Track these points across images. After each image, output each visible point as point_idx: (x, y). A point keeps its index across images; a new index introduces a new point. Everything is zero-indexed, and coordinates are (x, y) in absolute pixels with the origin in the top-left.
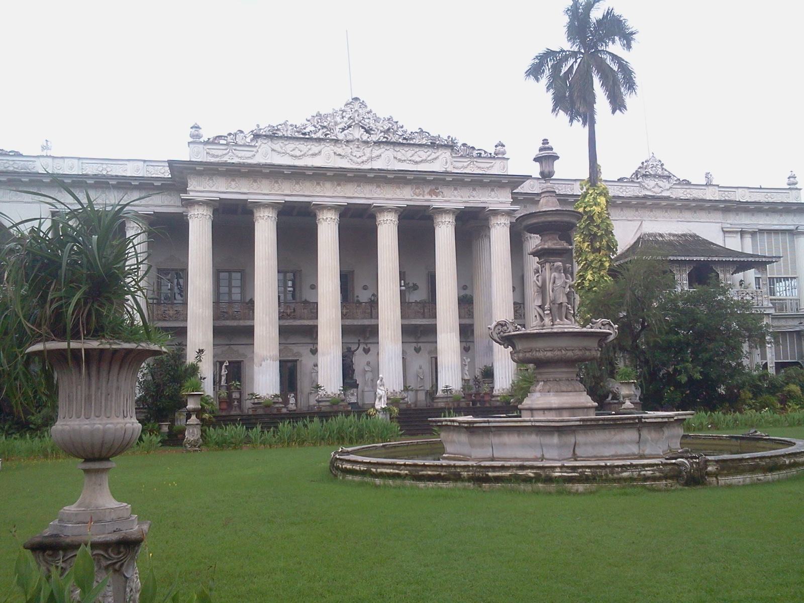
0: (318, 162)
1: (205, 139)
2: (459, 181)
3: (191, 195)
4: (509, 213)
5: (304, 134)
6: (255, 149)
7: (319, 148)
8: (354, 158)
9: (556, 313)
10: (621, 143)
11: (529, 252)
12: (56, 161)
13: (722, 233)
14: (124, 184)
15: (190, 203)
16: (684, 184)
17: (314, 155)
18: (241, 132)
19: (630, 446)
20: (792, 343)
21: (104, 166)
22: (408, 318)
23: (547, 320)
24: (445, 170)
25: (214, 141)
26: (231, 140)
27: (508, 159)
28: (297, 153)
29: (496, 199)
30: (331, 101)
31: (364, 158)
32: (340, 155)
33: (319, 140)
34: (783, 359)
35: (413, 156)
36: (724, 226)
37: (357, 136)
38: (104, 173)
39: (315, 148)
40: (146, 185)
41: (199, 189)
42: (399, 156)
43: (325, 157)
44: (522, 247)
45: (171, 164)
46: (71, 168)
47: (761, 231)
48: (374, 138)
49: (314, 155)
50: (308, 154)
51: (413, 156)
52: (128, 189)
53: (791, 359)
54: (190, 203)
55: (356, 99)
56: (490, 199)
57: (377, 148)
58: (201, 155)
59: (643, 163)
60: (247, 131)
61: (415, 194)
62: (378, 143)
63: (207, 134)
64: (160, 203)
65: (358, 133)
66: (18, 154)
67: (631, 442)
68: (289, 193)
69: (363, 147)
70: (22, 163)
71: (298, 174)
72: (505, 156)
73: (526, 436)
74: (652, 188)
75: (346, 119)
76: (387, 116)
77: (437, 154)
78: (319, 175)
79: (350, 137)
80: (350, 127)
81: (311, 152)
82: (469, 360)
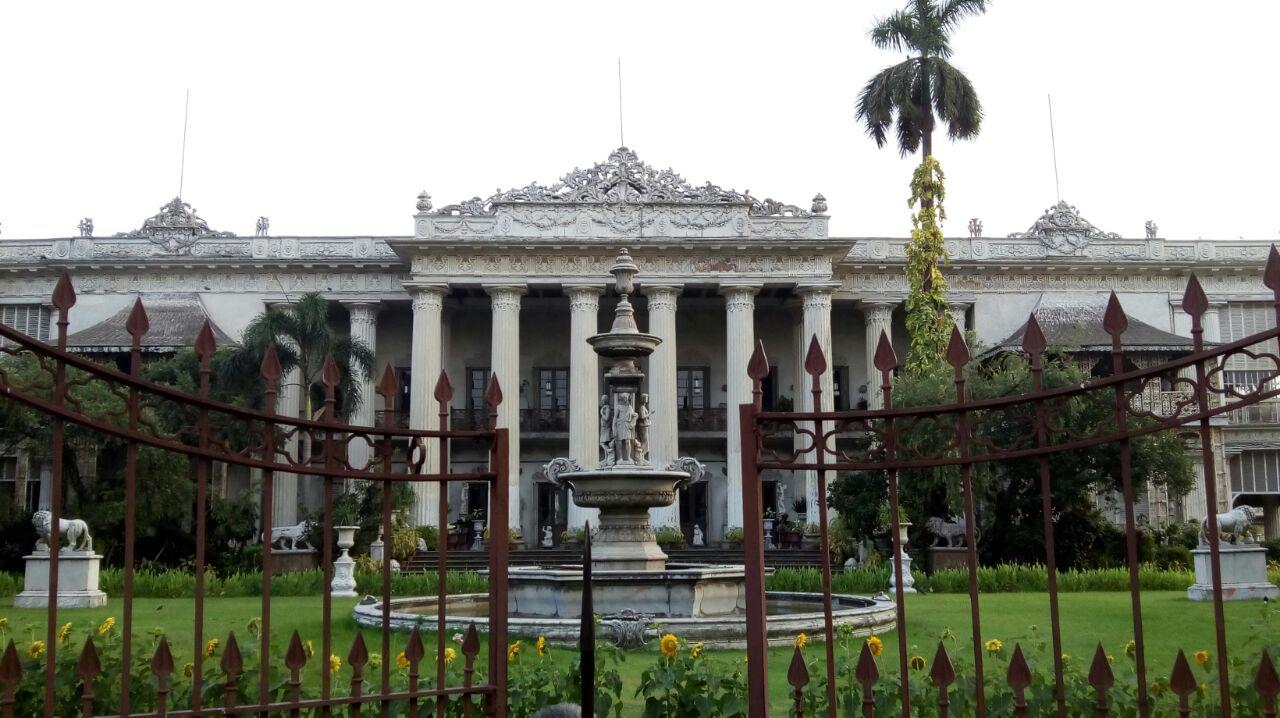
0: (570, 233)
1: (434, 209)
2: (758, 251)
3: (417, 281)
4: (827, 291)
5: (556, 198)
6: (493, 220)
7: (574, 214)
8: (618, 226)
9: (620, 451)
10: (992, 189)
11: (1121, 298)
12: (273, 242)
13: (1167, 309)
14: (346, 268)
15: (415, 291)
16: (1111, 240)
17: (565, 224)
18: (478, 199)
19: (657, 605)
20: (1260, 468)
21: (327, 246)
22: (695, 427)
23: (610, 459)
24: (738, 235)
25: (445, 213)
26: (470, 209)
27: (828, 218)
28: (546, 222)
29: (809, 272)
30: (594, 153)
31: (631, 225)
32: (600, 222)
33: (573, 205)
34: (1270, 490)
35: (696, 219)
36: (1172, 297)
37: (623, 197)
38: (326, 253)
39: (566, 215)
40: (370, 268)
41: (427, 273)
42: (678, 218)
43: (584, 227)
44: (865, 333)
45: (392, 242)
46: (288, 249)
47: (1235, 304)
48: (645, 199)
49: (565, 224)
50: (559, 222)
51: (696, 219)
52: (353, 272)
53: (1257, 490)
54: (415, 291)
55: (623, 149)
56: (802, 272)
57: (649, 210)
58: (430, 234)
59: (1047, 211)
60: (484, 198)
61: (698, 269)
62: (650, 205)
63: (437, 204)
64: (388, 289)
65: (622, 193)
66: (231, 236)
67: (659, 601)
68: (533, 273)
69: (628, 209)
70: (235, 245)
71: (543, 251)
72: (825, 213)
73: (544, 589)
74: (1061, 245)
75: (609, 176)
76: (666, 168)
77: (729, 215)
78: (570, 250)
79: (614, 200)
80: (615, 185)
81: (563, 220)
82: (785, 487)
